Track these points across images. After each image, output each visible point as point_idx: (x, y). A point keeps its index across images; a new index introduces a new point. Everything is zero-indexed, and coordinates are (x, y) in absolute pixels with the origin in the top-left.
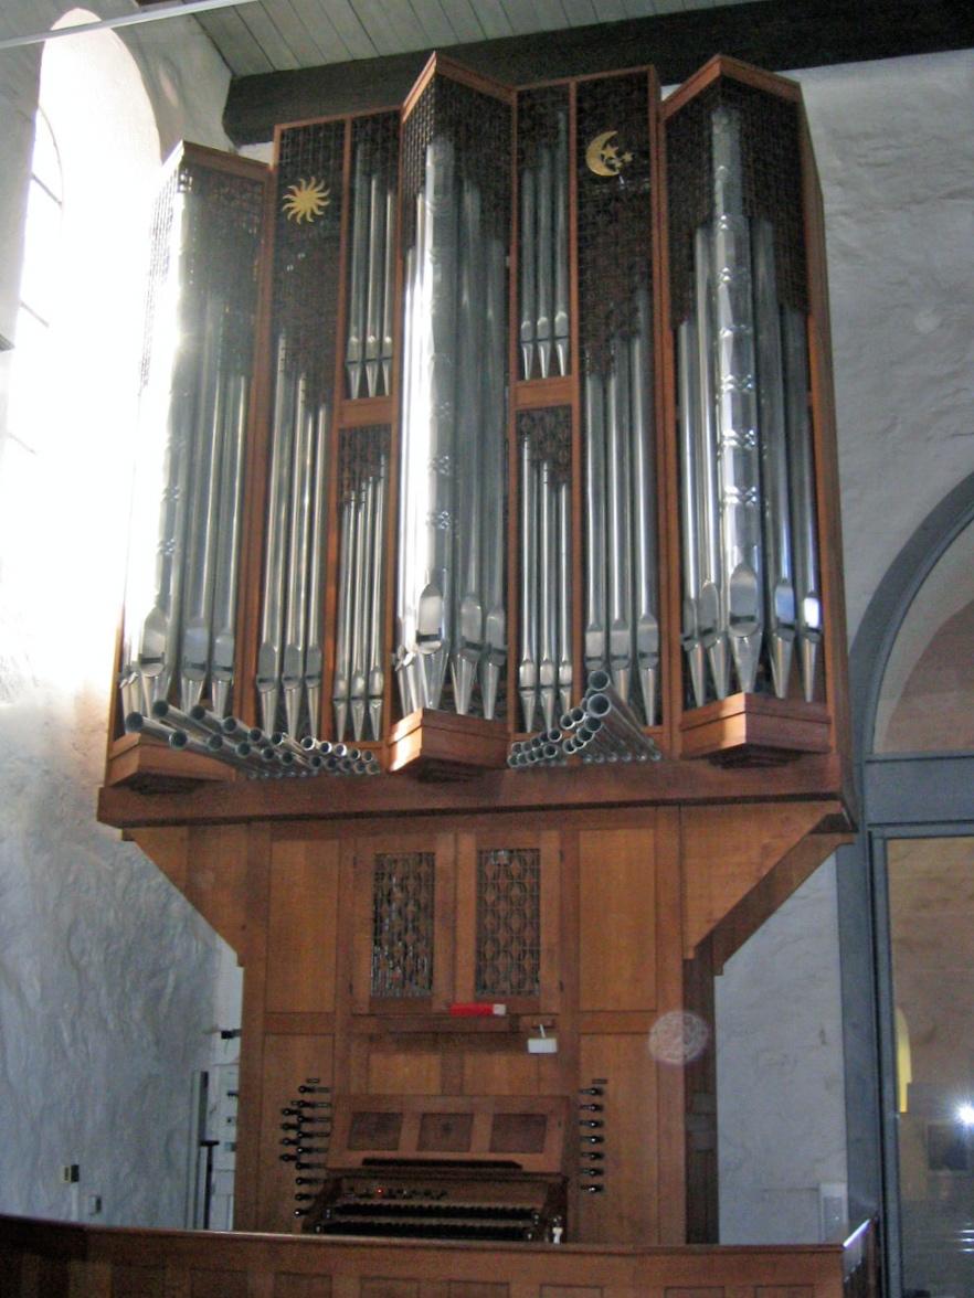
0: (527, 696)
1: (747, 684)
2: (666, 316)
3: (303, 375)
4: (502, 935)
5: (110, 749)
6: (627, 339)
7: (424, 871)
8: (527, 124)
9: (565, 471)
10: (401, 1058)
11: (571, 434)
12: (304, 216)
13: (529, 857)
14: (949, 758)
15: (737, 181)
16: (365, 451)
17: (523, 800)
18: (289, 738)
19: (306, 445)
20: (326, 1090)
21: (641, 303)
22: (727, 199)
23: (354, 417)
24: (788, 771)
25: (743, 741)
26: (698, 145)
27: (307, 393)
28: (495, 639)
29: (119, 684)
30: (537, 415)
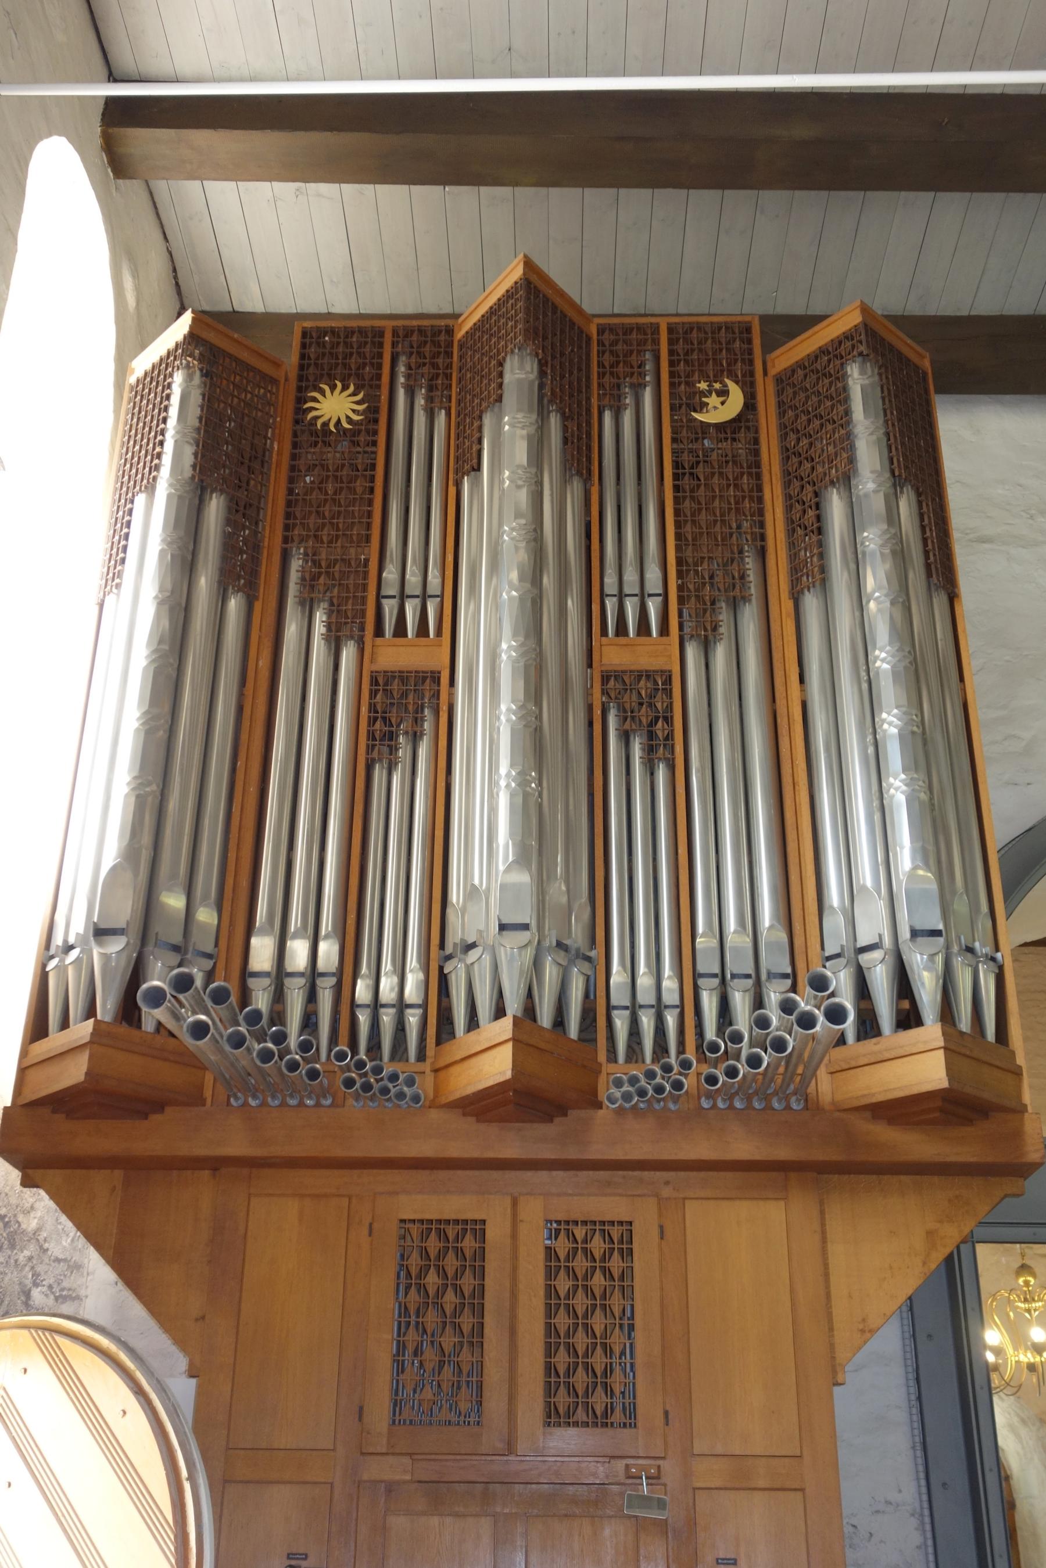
1: (513, 1006)
2: (785, 587)
3: (324, 605)
5: (24, 1053)
6: (735, 605)
8: (607, 359)
11: (671, 703)
12: (339, 421)
16: (404, 710)
17: (618, 1153)
19: (320, 677)
21: (750, 563)
23: (394, 656)
25: (945, 1084)
29: (44, 966)
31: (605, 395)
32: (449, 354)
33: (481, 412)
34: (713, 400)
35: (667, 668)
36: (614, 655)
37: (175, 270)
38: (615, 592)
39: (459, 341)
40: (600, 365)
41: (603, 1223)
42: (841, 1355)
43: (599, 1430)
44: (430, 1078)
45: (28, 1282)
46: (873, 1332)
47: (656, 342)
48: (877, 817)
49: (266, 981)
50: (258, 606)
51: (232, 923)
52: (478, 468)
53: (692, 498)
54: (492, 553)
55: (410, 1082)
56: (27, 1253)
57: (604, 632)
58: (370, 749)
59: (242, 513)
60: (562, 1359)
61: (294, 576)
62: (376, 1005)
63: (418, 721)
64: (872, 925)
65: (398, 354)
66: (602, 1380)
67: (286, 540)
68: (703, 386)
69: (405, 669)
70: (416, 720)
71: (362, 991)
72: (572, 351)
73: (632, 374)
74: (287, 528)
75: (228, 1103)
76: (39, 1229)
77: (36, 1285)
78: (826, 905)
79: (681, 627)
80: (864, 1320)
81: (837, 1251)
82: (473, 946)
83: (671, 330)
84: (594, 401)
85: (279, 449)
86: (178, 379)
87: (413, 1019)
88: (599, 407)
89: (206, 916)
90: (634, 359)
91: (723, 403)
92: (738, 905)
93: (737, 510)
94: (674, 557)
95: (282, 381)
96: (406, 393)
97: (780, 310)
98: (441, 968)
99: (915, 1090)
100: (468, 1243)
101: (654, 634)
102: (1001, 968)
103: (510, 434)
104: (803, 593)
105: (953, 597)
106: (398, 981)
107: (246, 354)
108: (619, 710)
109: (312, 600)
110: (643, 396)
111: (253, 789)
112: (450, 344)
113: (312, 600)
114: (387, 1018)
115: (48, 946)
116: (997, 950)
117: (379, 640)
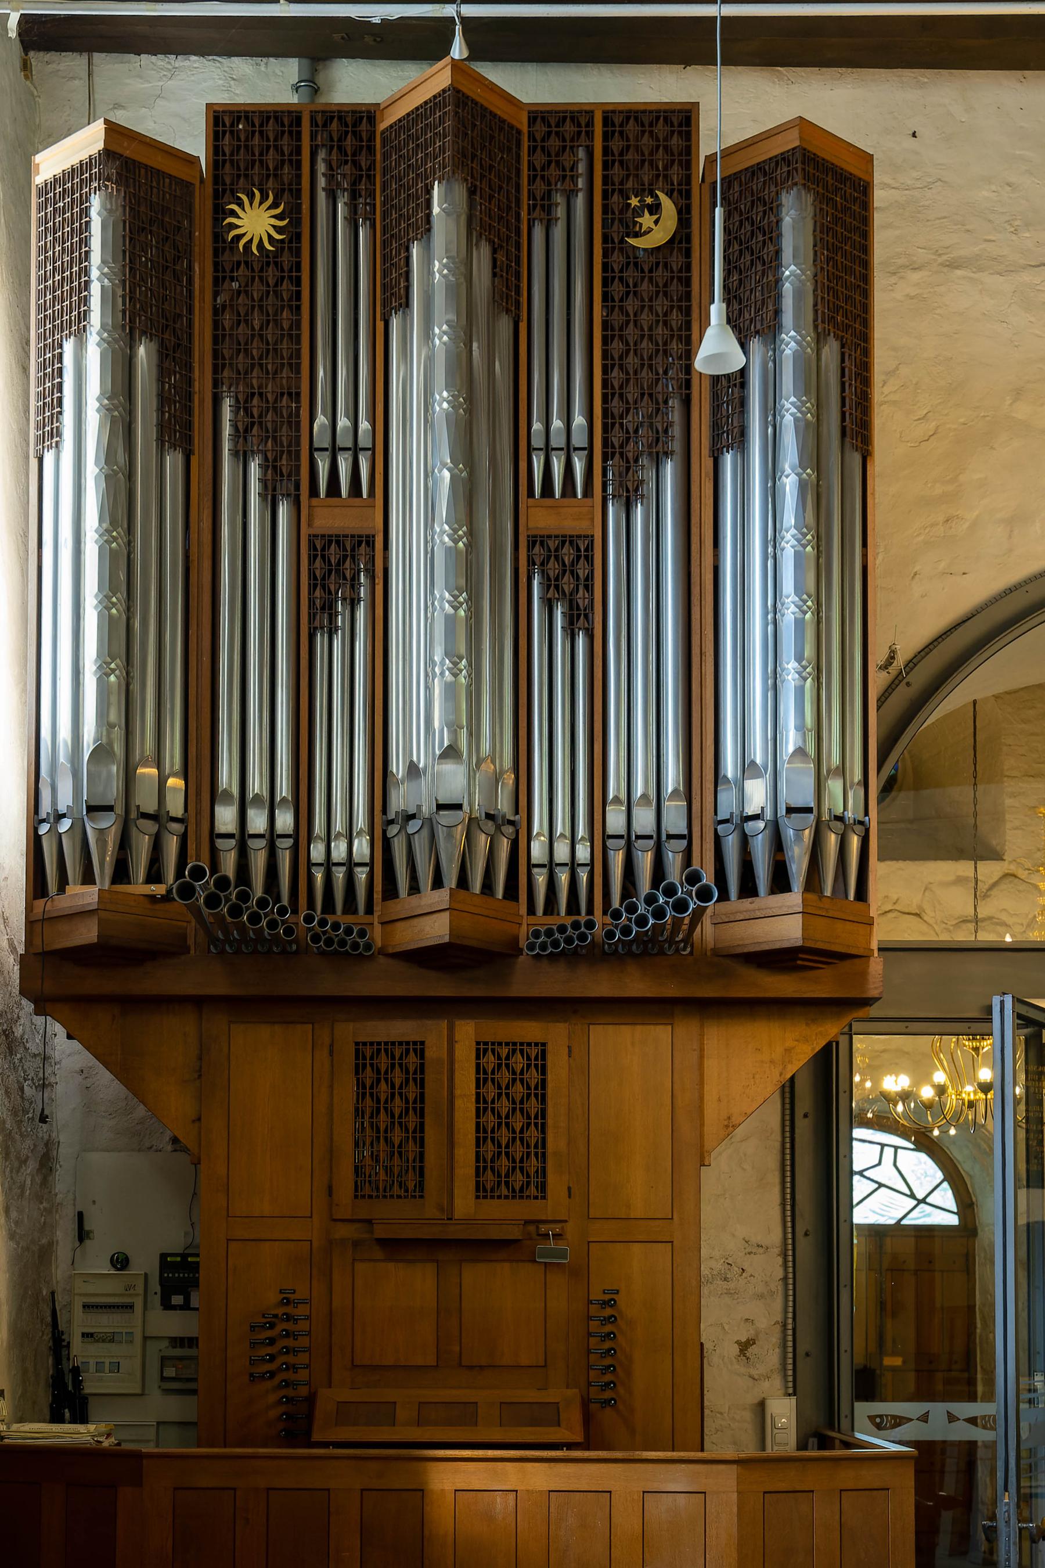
0: (362, 873)
1: (451, 879)
2: (706, 451)
4: (504, 1135)
8: (539, 159)
9: (582, 618)
10: (391, 1266)
15: (809, 286)
16: (342, 570)
18: (338, 914)
19: (260, 545)
20: (303, 1302)
23: (331, 519)
25: (447, 939)
26: (829, 229)
27: (263, 481)
28: (504, 805)
29: (36, 830)
30: (552, 544)
31: (535, 206)
32: (371, 150)
34: (646, 220)
35: (589, 533)
36: (540, 519)
39: (383, 133)
42: (708, 1145)
43: (517, 1201)
44: (378, 928)
47: (590, 135)
49: (233, 842)
50: (194, 460)
51: (198, 793)
52: (408, 304)
53: (621, 337)
55: (362, 933)
56: (19, 1056)
58: (312, 617)
59: (173, 359)
60: (490, 1148)
61: (227, 430)
65: (317, 146)
67: (216, 384)
68: (634, 202)
69: (341, 533)
70: (352, 587)
72: (502, 158)
73: (564, 177)
74: (216, 370)
75: (209, 951)
80: (729, 1118)
81: (711, 1065)
82: (413, 817)
83: (606, 121)
84: (524, 214)
86: (96, 203)
88: (529, 220)
89: (175, 783)
90: (566, 159)
91: (656, 222)
93: (665, 352)
94: (600, 452)
96: (327, 197)
98: (384, 832)
99: (777, 946)
102: (867, 830)
103: (435, 265)
104: (722, 453)
105: (866, 456)
108: (543, 576)
110: (575, 202)
112: (372, 137)
114: (339, 874)
117: (315, 501)
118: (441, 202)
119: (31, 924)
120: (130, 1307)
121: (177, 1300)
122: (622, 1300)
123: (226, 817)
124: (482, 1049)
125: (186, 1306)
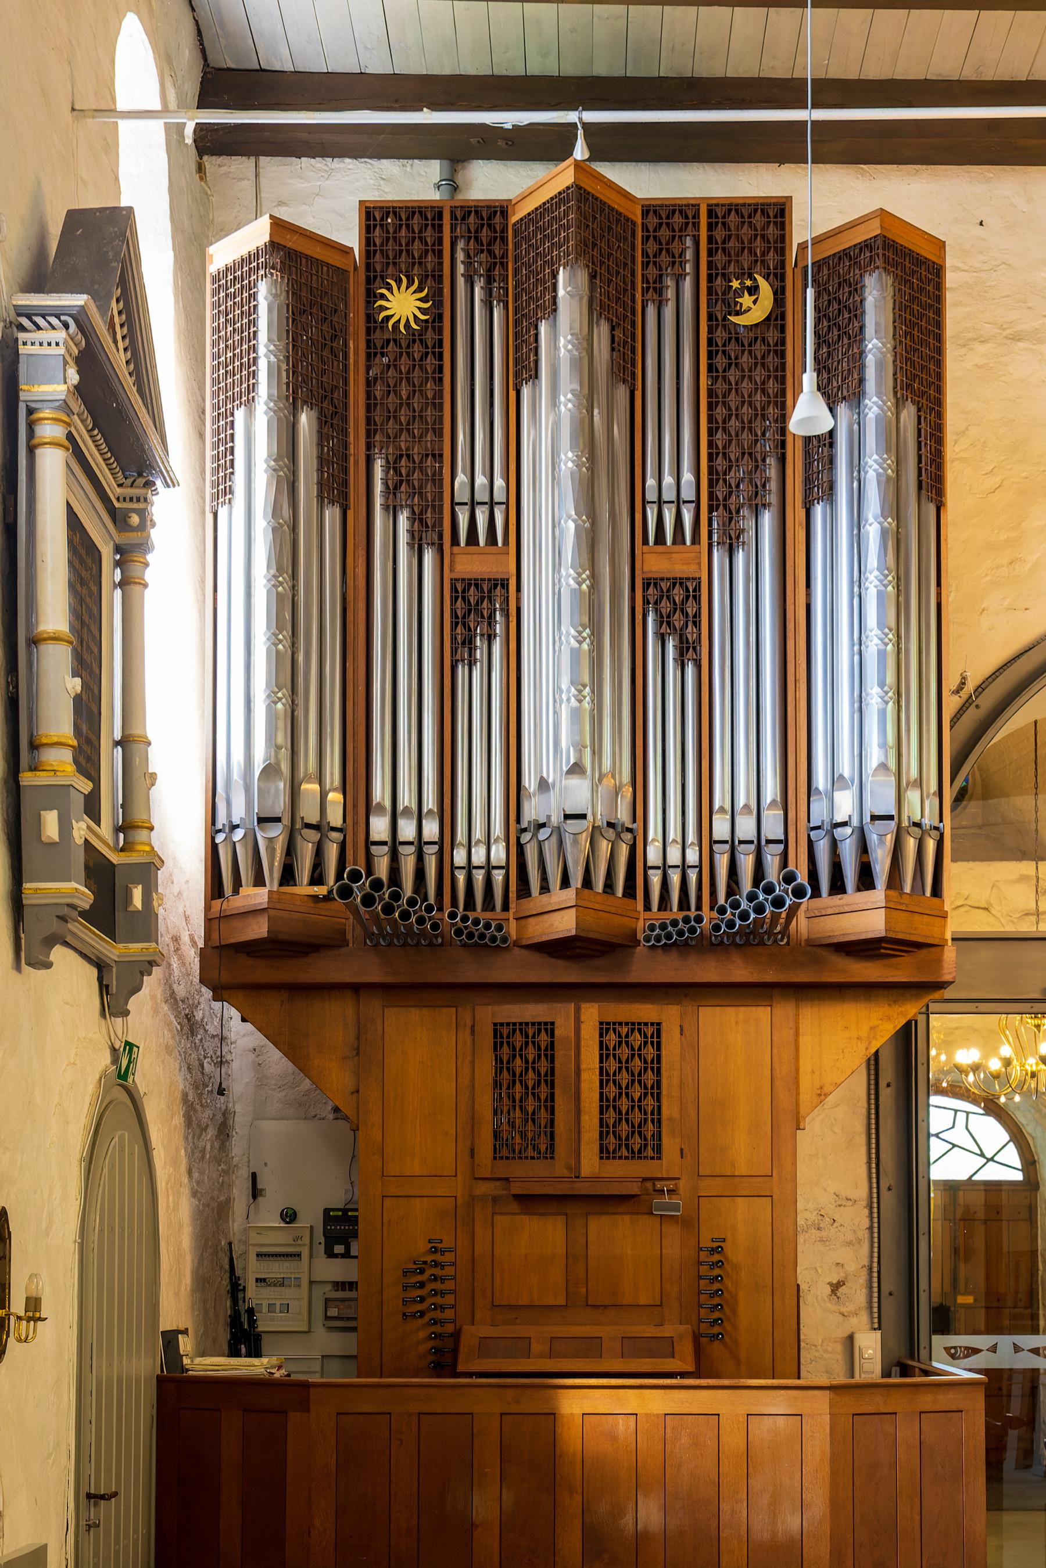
1: (577, 879)
2: (799, 503)
4: (624, 1104)
5: (208, 908)
7: (542, 1038)
10: (525, 1218)
13: (650, 1031)
14: (202, 44)
16: (479, 608)
19: (408, 586)
22: (879, 385)
23: (471, 565)
24: (906, 960)
27: (411, 532)
28: (623, 815)
29: (213, 838)
30: (664, 585)
32: (504, 240)
33: (537, 319)
34: (746, 300)
36: (654, 564)
37: (199, 33)
38: (656, 500)
39: (514, 225)
40: (645, 254)
41: (639, 1024)
44: (513, 924)
45: (202, 1057)
46: (826, 1095)
47: (696, 226)
48: (856, 716)
50: (350, 514)
51: (355, 806)
54: (544, 454)
55: (499, 928)
56: (199, 1037)
57: (645, 541)
59: (332, 424)
61: (378, 487)
62: (470, 867)
63: (491, 620)
64: (845, 805)
65: (456, 237)
66: (638, 1129)
67: (369, 446)
68: (735, 284)
70: (489, 624)
71: (460, 857)
73: (674, 263)
76: (202, 1020)
77: (205, 1057)
78: (814, 786)
79: (710, 537)
81: (805, 1042)
82: (543, 825)
83: (711, 213)
85: (356, 348)
86: (263, 289)
87: (498, 876)
88: (643, 301)
91: (755, 302)
92: (746, 777)
95: (352, 270)
96: (466, 282)
97: (833, 74)
98: (518, 839)
100: (544, 1037)
101: (688, 543)
102: (942, 835)
103: (564, 336)
106: (485, 849)
107: (318, 250)
109: (395, 507)
111: (362, 688)
112: (504, 230)
113: (395, 507)
114: (479, 876)
115: (214, 823)
116: (941, 821)
117: (456, 549)
118: (568, 286)
119: (208, 921)
120: (298, 1255)
121: (339, 1249)
122: (728, 1247)
123: (380, 827)
124: (605, 1028)
125: (347, 1255)
